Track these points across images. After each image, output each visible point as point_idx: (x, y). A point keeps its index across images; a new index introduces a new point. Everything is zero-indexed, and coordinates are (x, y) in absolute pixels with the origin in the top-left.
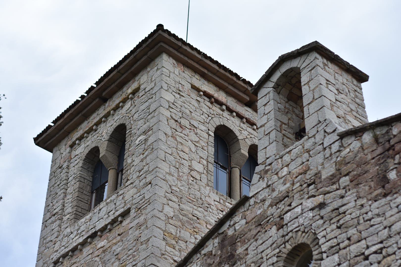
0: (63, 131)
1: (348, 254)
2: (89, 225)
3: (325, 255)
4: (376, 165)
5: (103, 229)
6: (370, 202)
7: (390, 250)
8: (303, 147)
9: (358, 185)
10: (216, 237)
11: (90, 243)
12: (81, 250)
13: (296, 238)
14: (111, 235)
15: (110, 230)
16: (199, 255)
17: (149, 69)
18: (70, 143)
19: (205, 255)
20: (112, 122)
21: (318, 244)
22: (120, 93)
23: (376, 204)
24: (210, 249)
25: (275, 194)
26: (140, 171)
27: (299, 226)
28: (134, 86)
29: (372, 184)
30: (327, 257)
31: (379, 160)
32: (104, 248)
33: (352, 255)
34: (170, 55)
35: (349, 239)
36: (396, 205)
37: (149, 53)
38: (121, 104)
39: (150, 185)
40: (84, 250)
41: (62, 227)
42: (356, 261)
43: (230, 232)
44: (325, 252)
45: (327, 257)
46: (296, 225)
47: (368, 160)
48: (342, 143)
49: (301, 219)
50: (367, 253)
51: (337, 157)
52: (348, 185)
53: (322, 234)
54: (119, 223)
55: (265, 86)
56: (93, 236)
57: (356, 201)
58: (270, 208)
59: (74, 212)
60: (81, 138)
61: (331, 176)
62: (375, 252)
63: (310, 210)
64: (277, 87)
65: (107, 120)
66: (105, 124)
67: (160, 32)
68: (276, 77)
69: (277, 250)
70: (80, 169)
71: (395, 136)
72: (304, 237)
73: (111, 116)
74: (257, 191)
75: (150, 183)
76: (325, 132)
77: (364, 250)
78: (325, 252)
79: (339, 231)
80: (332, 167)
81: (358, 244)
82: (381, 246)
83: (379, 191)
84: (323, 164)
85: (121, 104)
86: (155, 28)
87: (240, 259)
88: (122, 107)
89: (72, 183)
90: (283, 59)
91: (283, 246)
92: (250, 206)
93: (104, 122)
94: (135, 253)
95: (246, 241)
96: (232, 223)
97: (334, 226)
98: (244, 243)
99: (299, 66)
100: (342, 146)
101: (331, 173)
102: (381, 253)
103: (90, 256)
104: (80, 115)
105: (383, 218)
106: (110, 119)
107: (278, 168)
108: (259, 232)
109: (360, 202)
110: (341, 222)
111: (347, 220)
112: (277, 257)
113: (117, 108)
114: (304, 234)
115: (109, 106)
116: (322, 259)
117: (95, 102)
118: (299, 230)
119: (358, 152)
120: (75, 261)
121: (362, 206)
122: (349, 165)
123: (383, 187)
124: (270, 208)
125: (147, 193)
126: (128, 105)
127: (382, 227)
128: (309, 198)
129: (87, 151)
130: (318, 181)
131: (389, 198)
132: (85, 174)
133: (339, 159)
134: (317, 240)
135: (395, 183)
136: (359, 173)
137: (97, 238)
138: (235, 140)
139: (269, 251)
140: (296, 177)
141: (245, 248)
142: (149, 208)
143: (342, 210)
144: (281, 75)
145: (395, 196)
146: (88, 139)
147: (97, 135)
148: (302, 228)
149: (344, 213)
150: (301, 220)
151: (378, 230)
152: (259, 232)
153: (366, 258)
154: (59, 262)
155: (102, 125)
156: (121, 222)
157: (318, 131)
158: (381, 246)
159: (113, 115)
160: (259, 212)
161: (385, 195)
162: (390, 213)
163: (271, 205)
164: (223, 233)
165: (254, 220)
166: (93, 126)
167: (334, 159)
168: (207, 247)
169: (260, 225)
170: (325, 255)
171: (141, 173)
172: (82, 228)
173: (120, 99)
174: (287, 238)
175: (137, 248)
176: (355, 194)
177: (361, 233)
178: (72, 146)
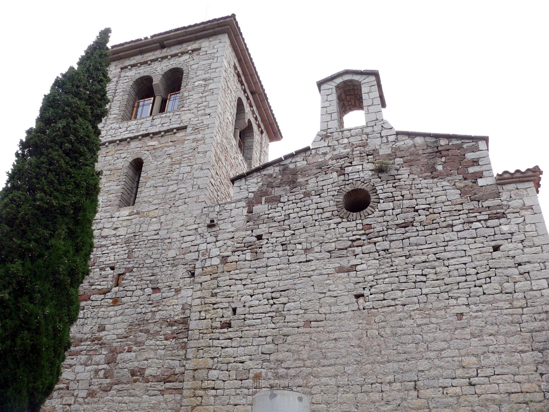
0: (117, 55)
1: (401, 205)
2: (141, 127)
3: (381, 201)
4: (426, 158)
5: (155, 134)
6: (421, 179)
7: (436, 211)
8: (362, 131)
9: (411, 166)
10: (277, 166)
11: (140, 140)
12: (129, 142)
13: (356, 184)
14: (163, 140)
15: (162, 136)
16: (259, 174)
17: (211, 39)
18: (121, 66)
19: (265, 175)
20: (168, 64)
21: (376, 192)
22: (180, 47)
23: (426, 181)
24: (272, 173)
25: (335, 153)
26: (198, 104)
27: (359, 178)
28: (195, 45)
29: (423, 168)
30: (384, 202)
31: (429, 156)
32: (155, 147)
33: (404, 206)
34: (230, 37)
35: (403, 196)
36: (442, 186)
37: (216, 29)
38: (180, 54)
39: (209, 116)
40: (132, 143)
41: (108, 122)
42: (408, 210)
43: (292, 166)
44: (381, 199)
45: (384, 202)
46: (358, 176)
47: (420, 153)
48: (397, 138)
49: (362, 174)
50: (417, 208)
51: (393, 145)
52: (402, 164)
53: (380, 187)
54: (173, 133)
55: (328, 83)
56: (147, 135)
57: (409, 175)
58: (331, 160)
59: (122, 115)
60: (133, 66)
61: (388, 154)
62: (424, 209)
63: (370, 170)
64: (337, 87)
65: (162, 61)
66: (160, 63)
67: (232, 18)
68: (339, 81)
69: (338, 188)
70: (130, 86)
71: (442, 146)
72: (363, 185)
73: (167, 59)
74: (318, 147)
75: (209, 115)
76: (382, 127)
77: (414, 206)
78: (381, 199)
79: (394, 189)
80: (389, 149)
81: (410, 201)
82: (428, 206)
83: (430, 174)
84: (380, 145)
85: (180, 54)
86: (230, 15)
87: (301, 185)
88: (180, 57)
89: (121, 94)
90: (347, 72)
91: (344, 186)
92: (311, 154)
93: (160, 61)
94: (192, 158)
95: (307, 175)
96: (293, 161)
97: (391, 185)
98: (304, 176)
99: (360, 80)
100: (397, 139)
101: (388, 153)
102: (428, 210)
103: (139, 149)
104: (138, 49)
105: (431, 191)
106: (165, 61)
107: (339, 137)
108: (319, 172)
109: (412, 176)
110: (397, 184)
111: (402, 184)
112: (338, 192)
113: (176, 55)
114: (363, 184)
115: (166, 52)
116: (379, 203)
117: (155, 45)
118: (360, 180)
119: (411, 147)
120: (121, 148)
121: (414, 179)
122: (402, 152)
123: (432, 173)
124: (331, 160)
125: (207, 120)
126: (186, 57)
127: (430, 196)
128: (368, 162)
129: (138, 76)
130: (375, 154)
131: (435, 180)
132: (132, 92)
133: (394, 146)
134: (375, 191)
135: (440, 171)
136: (412, 159)
137: (148, 138)
138: (243, 111)
139: (330, 186)
140: (356, 147)
141: (305, 180)
142: (207, 131)
143: (397, 177)
144: (342, 82)
145: (441, 180)
146: (140, 68)
147: (151, 68)
148: (362, 180)
149: (399, 179)
150: (362, 175)
151: (427, 196)
152: (319, 172)
153: (417, 211)
154: (104, 145)
155: (157, 63)
156: (175, 133)
157: (376, 125)
158: (428, 206)
159: (170, 59)
160: (320, 160)
161: (433, 178)
162: (437, 189)
163: (332, 159)
164: (284, 165)
165: (315, 164)
166: (149, 61)
167: (391, 145)
168: (268, 170)
169: (321, 168)
170: (381, 201)
171: (199, 106)
172: (132, 127)
173: (180, 51)
174: (347, 182)
175: (193, 154)
176: (409, 171)
177: (412, 195)
178: (122, 69)
